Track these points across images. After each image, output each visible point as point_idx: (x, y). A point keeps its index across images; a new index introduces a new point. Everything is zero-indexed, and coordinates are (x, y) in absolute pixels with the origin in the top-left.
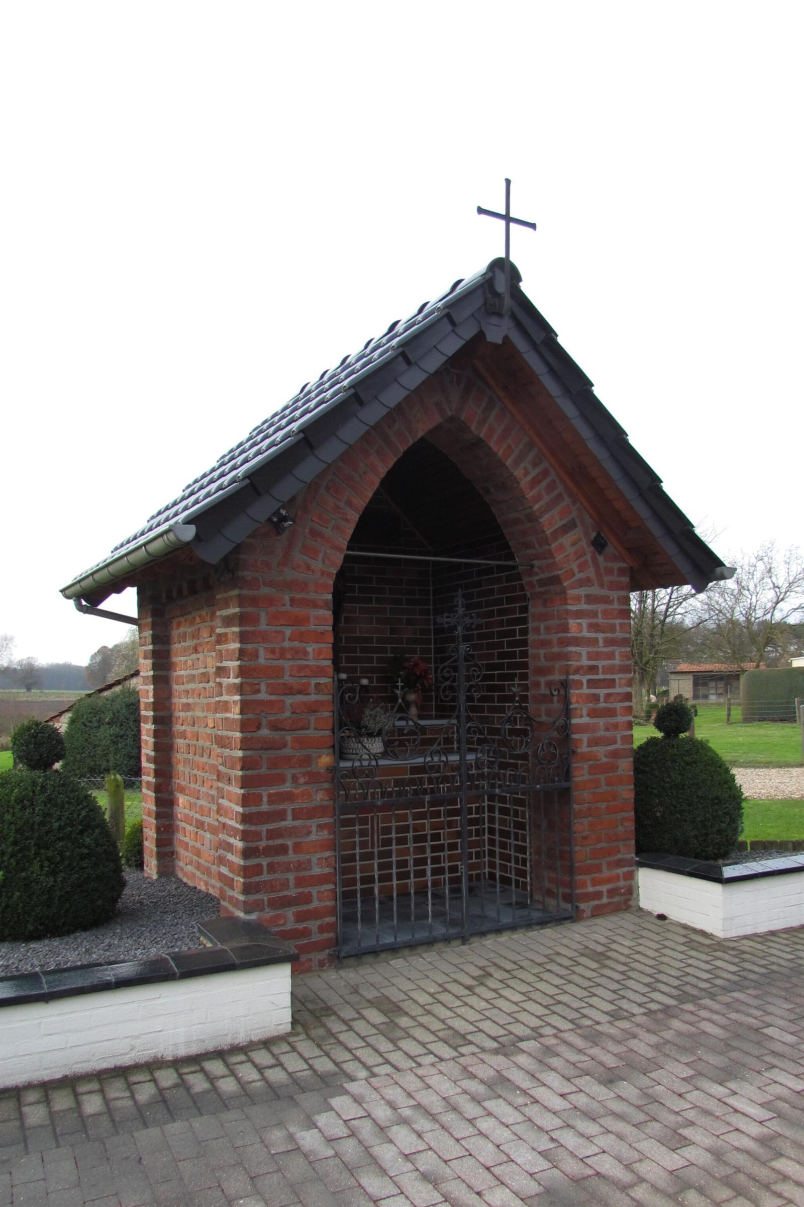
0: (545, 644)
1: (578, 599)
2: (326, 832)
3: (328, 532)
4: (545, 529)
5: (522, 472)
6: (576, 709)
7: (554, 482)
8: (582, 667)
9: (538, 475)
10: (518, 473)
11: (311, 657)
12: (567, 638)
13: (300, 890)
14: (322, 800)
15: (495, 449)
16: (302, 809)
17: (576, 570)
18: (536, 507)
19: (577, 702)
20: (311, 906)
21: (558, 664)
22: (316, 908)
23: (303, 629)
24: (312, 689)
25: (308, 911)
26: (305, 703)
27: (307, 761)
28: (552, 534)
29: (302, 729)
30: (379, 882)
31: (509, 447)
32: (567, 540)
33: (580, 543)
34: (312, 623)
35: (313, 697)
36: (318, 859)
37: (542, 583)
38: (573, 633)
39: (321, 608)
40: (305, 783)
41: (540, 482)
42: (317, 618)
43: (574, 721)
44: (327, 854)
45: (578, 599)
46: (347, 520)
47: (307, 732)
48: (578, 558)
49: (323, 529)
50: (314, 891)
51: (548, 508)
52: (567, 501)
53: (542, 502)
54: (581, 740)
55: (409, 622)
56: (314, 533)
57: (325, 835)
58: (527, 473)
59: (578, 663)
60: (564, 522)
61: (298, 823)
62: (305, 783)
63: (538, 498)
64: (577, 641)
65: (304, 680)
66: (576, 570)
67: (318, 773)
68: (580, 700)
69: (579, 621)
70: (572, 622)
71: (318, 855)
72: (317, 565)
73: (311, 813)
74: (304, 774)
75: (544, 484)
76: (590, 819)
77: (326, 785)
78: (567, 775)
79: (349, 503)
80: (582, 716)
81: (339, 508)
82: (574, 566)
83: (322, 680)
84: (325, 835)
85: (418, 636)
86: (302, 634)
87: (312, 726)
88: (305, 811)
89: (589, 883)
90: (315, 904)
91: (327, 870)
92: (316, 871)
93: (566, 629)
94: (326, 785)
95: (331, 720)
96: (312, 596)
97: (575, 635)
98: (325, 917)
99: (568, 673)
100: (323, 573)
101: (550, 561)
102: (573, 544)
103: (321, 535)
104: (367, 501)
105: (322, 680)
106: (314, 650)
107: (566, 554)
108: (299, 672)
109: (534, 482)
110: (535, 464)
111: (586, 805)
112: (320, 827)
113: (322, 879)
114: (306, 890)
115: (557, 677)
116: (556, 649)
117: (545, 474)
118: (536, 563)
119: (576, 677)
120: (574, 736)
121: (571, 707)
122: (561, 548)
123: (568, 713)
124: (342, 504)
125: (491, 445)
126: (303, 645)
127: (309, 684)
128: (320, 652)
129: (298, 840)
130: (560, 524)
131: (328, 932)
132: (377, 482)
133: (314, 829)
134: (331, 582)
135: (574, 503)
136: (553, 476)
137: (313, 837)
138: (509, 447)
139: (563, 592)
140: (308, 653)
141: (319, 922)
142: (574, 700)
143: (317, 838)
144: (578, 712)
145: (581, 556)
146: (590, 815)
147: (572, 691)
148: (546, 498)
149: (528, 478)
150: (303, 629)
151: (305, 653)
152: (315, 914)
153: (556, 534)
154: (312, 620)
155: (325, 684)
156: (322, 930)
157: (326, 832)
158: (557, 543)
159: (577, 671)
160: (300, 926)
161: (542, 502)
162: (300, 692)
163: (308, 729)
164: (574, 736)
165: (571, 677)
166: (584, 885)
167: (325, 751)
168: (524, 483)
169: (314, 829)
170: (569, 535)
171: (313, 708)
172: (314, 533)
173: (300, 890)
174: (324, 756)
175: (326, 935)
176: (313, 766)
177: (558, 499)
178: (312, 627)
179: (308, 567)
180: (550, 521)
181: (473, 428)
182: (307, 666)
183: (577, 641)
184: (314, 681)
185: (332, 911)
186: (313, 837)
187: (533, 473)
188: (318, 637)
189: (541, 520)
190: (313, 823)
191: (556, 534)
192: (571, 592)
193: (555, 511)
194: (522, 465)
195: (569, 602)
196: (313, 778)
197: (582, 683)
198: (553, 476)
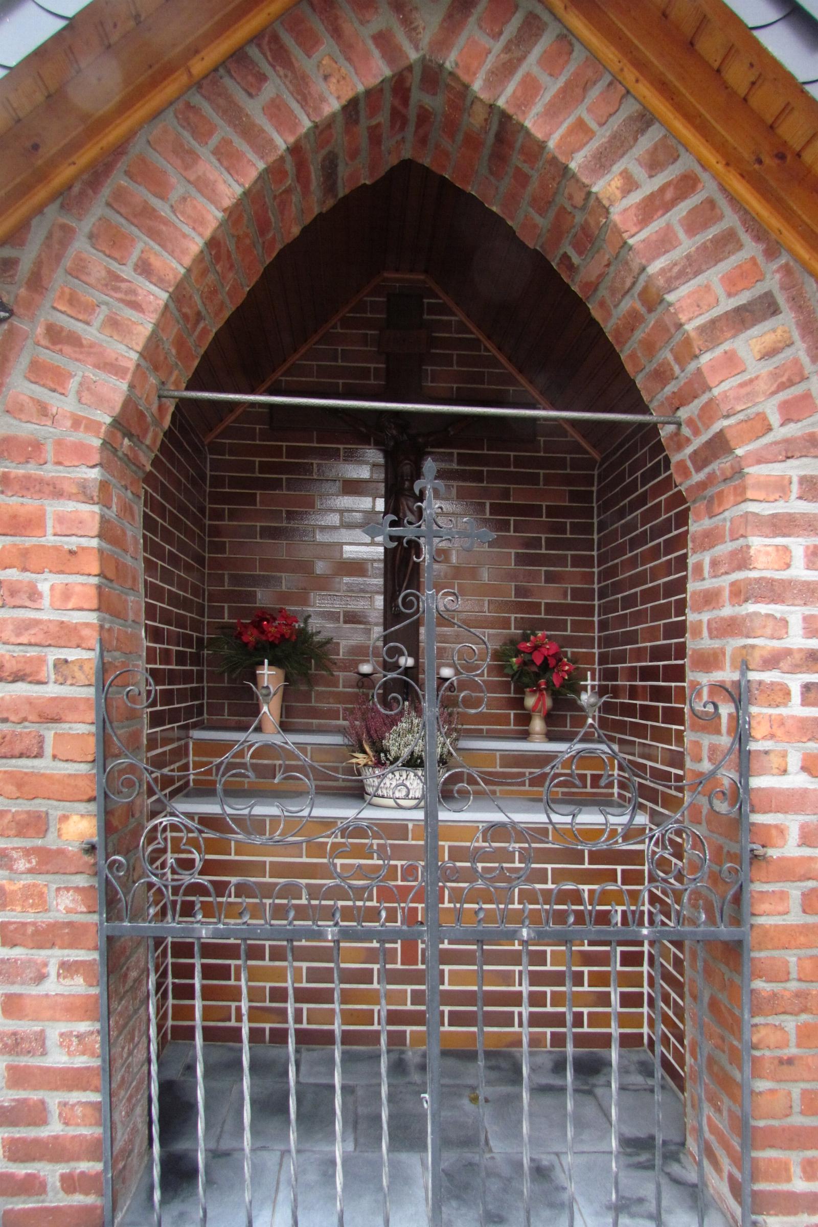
0: (710, 599)
1: (781, 487)
2: (79, 980)
3: (91, 333)
4: (683, 318)
5: (617, 183)
6: (766, 753)
7: (711, 203)
8: (788, 652)
9: (662, 190)
10: (605, 186)
11: (46, 602)
12: (749, 581)
13: (22, 1094)
14: (69, 911)
15: (538, 134)
16: (24, 924)
17: (775, 419)
18: (654, 268)
19: (772, 736)
20: (43, 1133)
21: (733, 644)
22: (56, 1138)
23: (28, 542)
24: (49, 671)
25: (36, 1141)
26: (30, 702)
27: (36, 824)
28: (702, 329)
29: (21, 756)
30: (343, 1043)
31: (580, 125)
32: (748, 344)
33: (788, 353)
34: (50, 530)
35: (52, 690)
36: (62, 1035)
37: (702, 458)
38: (764, 567)
39: (70, 497)
40: (30, 871)
41: (668, 207)
42: (60, 519)
43: (756, 782)
44: (84, 1027)
45: (781, 487)
46: (135, 306)
47: (36, 762)
48: (782, 387)
49: (78, 327)
50: (54, 1099)
51: (692, 266)
52: (751, 249)
53: (677, 254)
54: (781, 831)
55: (551, 578)
56: (56, 336)
57: (78, 986)
58: (630, 185)
59: (776, 644)
60: (743, 299)
61: (239, 900)
62: (30, 871)
63: (665, 243)
64: (774, 591)
65: (32, 652)
66: (775, 419)
67: (60, 852)
68: (779, 732)
69: (780, 541)
70: (757, 543)
71: (64, 1027)
72: (65, 404)
73: (46, 936)
74: (28, 852)
75: (683, 208)
76: (804, 1017)
77: (82, 881)
78: (738, 905)
79: (145, 269)
80: (785, 772)
81: (118, 278)
82: (771, 410)
83: (72, 655)
84: (78, 986)
85: (569, 601)
86: (25, 553)
87: (49, 750)
88: (30, 930)
89: (796, 1170)
90: (54, 1128)
91: (81, 1061)
92: (58, 1059)
93: (742, 560)
94: (82, 881)
95: (92, 741)
96: (50, 471)
97: (768, 574)
98: (78, 1159)
99: (745, 667)
100: (77, 423)
101: (704, 398)
102: (769, 354)
103: (74, 340)
104: (188, 261)
105: (72, 655)
106: (52, 588)
107: (746, 377)
108: (18, 635)
109: (651, 208)
110: (653, 166)
111: (793, 985)
112: (67, 969)
113: (71, 1079)
114: (34, 1096)
115: (727, 675)
116: (727, 611)
117: (686, 184)
118: (683, 414)
119: (768, 677)
120: (757, 818)
121: (753, 746)
122: (731, 361)
123: (745, 762)
124: (127, 272)
125: (528, 124)
126: (28, 576)
127: (42, 660)
128: (67, 593)
129: (16, 989)
130: (728, 304)
131: (87, 1193)
132: (214, 216)
133: (52, 970)
134: (97, 443)
135: (771, 253)
136: (708, 188)
137: (52, 986)
138: (580, 125)
139: (738, 472)
140: (40, 595)
141: (63, 1168)
142: (758, 732)
143: (60, 990)
144: (775, 761)
145: (791, 383)
146: (804, 1010)
147: (754, 710)
148: (687, 245)
149: (636, 197)
150: (28, 542)
151: (34, 595)
152: (53, 1151)
153: (713, 331)
154: (50, 523)
155: (80, 663)
156: (70, 1184)
157: (79, 980)
158: (719, 351)
159: (772, 661)
160: (21, 1170)
161: (677, 254)
162: (18, 677)
163: (39, 755)
164: (757, 818)
165: (753, 676)
166: (782, 1172)
167: (82, 807)
168: (622, 210)
169: (52, 970)
170: (755, 331)
171: (50, 715)
172: (56, 336)
173: (22, 1094)
174: (75, 818)
175: (78, 1199)
176: (52, 835)
177: (725, 244)
178: (50, 540)
179: (43, 410)
180: (698, 300)
181: (477, 86)
182: (37, 622)
183: (774, 591)
184: (53, 655)
185: (93, 1150)
186: (52, 986)
187: (650, 186)
188: (67, 560)
189: (670, 298)
190: (53, 957)
191: (713, 331)
192: (755, 471)
193: (714, 276)
194: (617, 168)
195: (750, 494)
196: (48, 861)
197: (788, 693)
198: (708, 188)
